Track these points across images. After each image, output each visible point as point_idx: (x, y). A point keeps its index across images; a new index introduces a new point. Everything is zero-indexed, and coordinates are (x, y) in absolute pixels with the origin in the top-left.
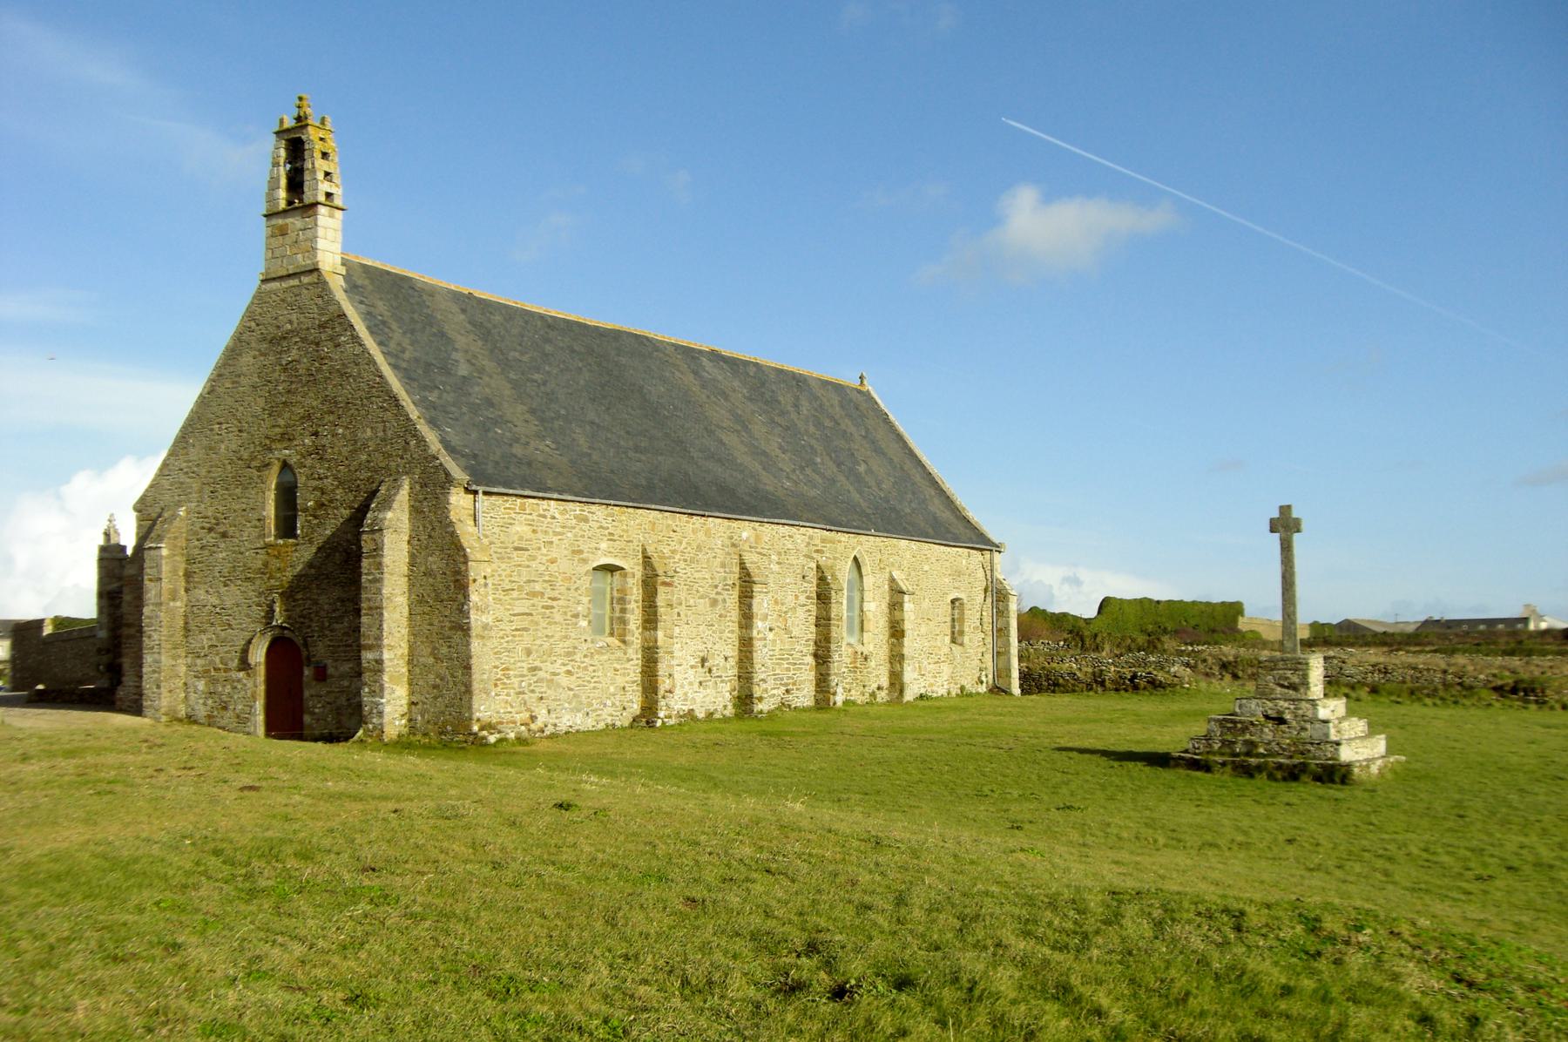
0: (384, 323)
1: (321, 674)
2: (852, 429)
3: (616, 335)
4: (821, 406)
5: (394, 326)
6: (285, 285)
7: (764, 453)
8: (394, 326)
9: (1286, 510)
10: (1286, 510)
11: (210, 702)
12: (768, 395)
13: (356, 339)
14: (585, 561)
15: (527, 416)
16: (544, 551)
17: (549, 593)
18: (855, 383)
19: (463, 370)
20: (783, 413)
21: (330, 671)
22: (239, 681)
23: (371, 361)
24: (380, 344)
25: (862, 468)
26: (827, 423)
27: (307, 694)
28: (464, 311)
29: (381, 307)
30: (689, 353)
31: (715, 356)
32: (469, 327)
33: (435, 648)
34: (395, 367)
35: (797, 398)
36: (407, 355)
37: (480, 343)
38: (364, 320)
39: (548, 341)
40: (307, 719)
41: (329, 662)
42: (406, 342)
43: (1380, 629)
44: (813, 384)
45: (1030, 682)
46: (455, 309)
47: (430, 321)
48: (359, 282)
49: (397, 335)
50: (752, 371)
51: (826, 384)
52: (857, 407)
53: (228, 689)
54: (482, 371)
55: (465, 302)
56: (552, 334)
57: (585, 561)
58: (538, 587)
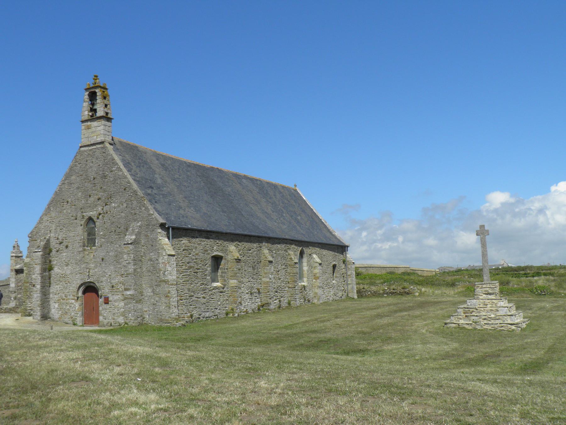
0: (129, 163)
1: (107, 301)
2: (294, 204)
3: (212, 169)
4: (283, 195)
5: (133, 164)
6: (90, 148)
7: (266, 212)
8: (133, 164)
9: (482, 227)
10: (482, 227)
11: (60, 312)
12: (265, 192)
13: (119, 169)
14: (208, 254)
15: (184, 199)
16: (194, 250)
17: (196, 266)
18: (293, 187)
19: (159, 181)
20: (271, 198)
21: (110, 299)
22: (72, 304)
23: (125, 177)
24: (128, 171)
25: (299, 218)
26: (286, 201)
27: (100, 308)
28: (157, 159)
29: (128, 157)
30: (237, 176)
31: (246, 177)
32: (160, 165)
33: (154, 289)
34: (134, 180)
35: (275, 192)
36: (138, 175)
37: (164, 172)
38: (122, 162)
39: (188, 171)
40: (101, 318)
41: (109, 295)
42: (138, 171)
43: (425, 274)
44: (279, 187)
45: (360, 293)
46: (154, 159)
47: (145, 163)
48: (119, 148)
49: (134, 168)
50: (259, 182)
51: (283, 187)
52: (294, 195)
53: (68, 307)
54: (166, 182)
55: (158, 156)
56: (189, 169)
57: (208, 254)
58: (192, 264)
